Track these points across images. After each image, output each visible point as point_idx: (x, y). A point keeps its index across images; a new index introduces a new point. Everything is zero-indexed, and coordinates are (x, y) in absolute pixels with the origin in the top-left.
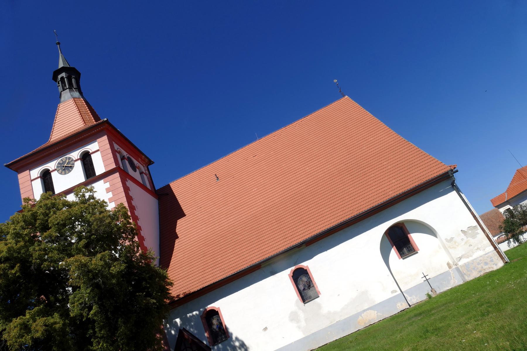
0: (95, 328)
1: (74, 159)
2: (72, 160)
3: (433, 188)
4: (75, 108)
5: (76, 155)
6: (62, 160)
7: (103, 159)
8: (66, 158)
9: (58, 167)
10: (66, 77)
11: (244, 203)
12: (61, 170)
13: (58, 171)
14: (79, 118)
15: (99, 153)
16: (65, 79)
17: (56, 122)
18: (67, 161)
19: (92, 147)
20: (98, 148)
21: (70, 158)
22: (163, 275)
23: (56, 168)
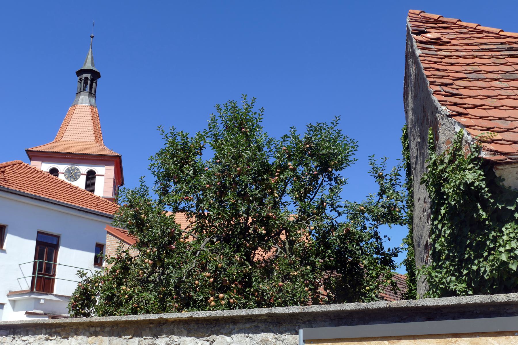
0: (465, 251)
1: (81, 173)
2: (80, 172)
3: (109, 219)
4: (89, 113)
5: (84, 169)
6: (71, 167)
7: (104, 185)
8: (76, 168)
9: (66, 171)
10: (90, 80)
11: (72, 137)
12: (67, 176)
13: (65, 175)
14: (91, 128)
15: (103, 177)
16: (89, 81)
17: (70, 122)
18: (76, 171)
19: (99, 170)
20: (103, 174)
21: (78, 169)
22: (437, 113)
23: (64, 172)
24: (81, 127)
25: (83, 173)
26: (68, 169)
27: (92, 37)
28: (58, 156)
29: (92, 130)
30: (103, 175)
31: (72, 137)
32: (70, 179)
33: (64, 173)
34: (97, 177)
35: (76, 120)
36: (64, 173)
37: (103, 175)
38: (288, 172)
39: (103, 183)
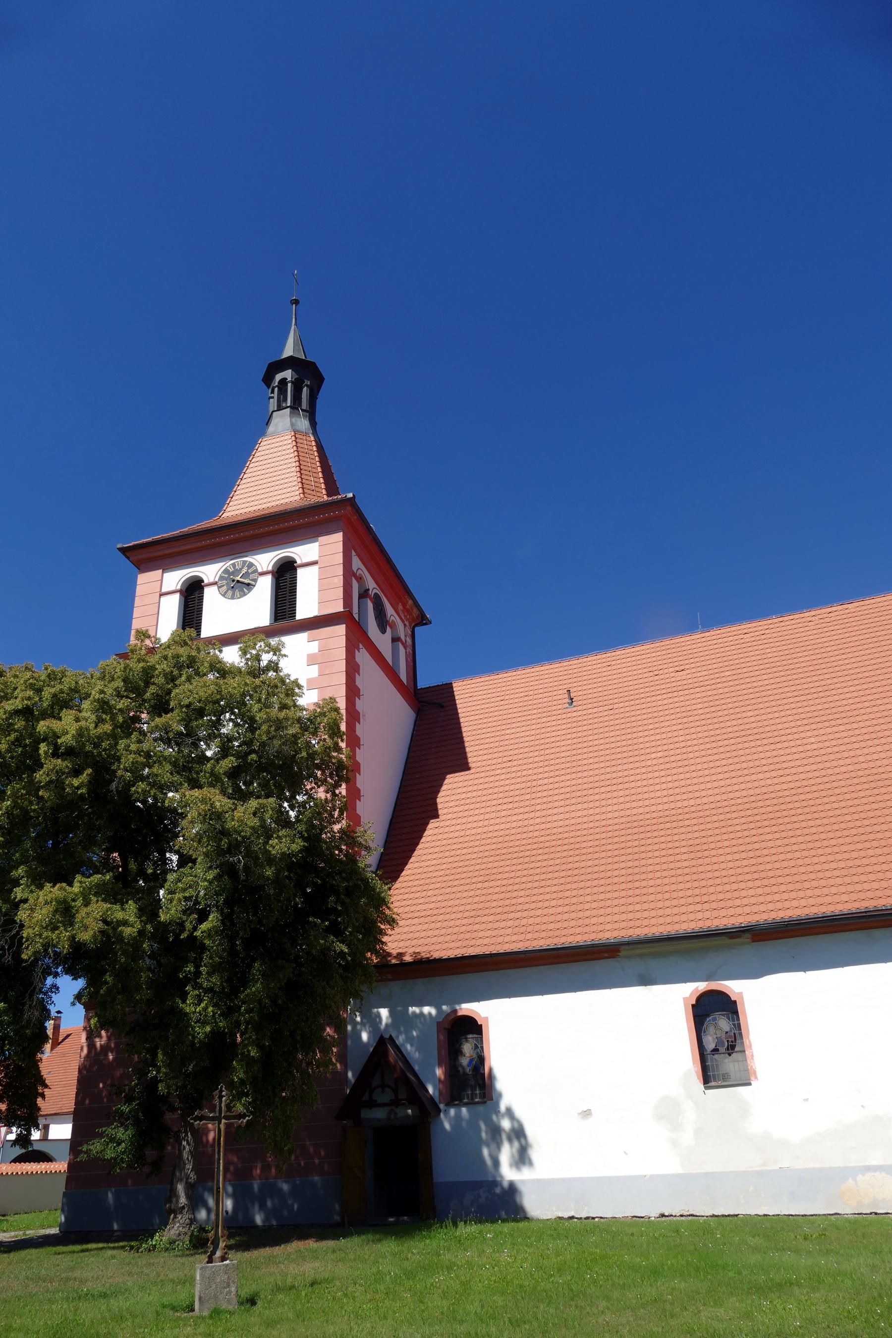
1: (260, 570)
5: (265, 560)
6: (234, 565)
7: (320, 585)
8: (244, 562)
9: (221, 578)
10: (292, 382)
11: (614, 769)
13: (219, 588)
15: (315, 568)
16: (289, 385)
20: (315, 557)
21: (251, 565)
23: (217, 580)
24: (522, 745)
25: (265, 570)
26: (226, 571)
27: (296, 302)
28: (199, 544)
29: (295, 483)
30: (314, 563)
31: (614, 769)
32: (233, 594)
33: (215, 583)
34: (300, 572)
35: (284, 491)
36: (215, 583)
37: (314, 563)
38: (197, 694)
39: (298, 578)
